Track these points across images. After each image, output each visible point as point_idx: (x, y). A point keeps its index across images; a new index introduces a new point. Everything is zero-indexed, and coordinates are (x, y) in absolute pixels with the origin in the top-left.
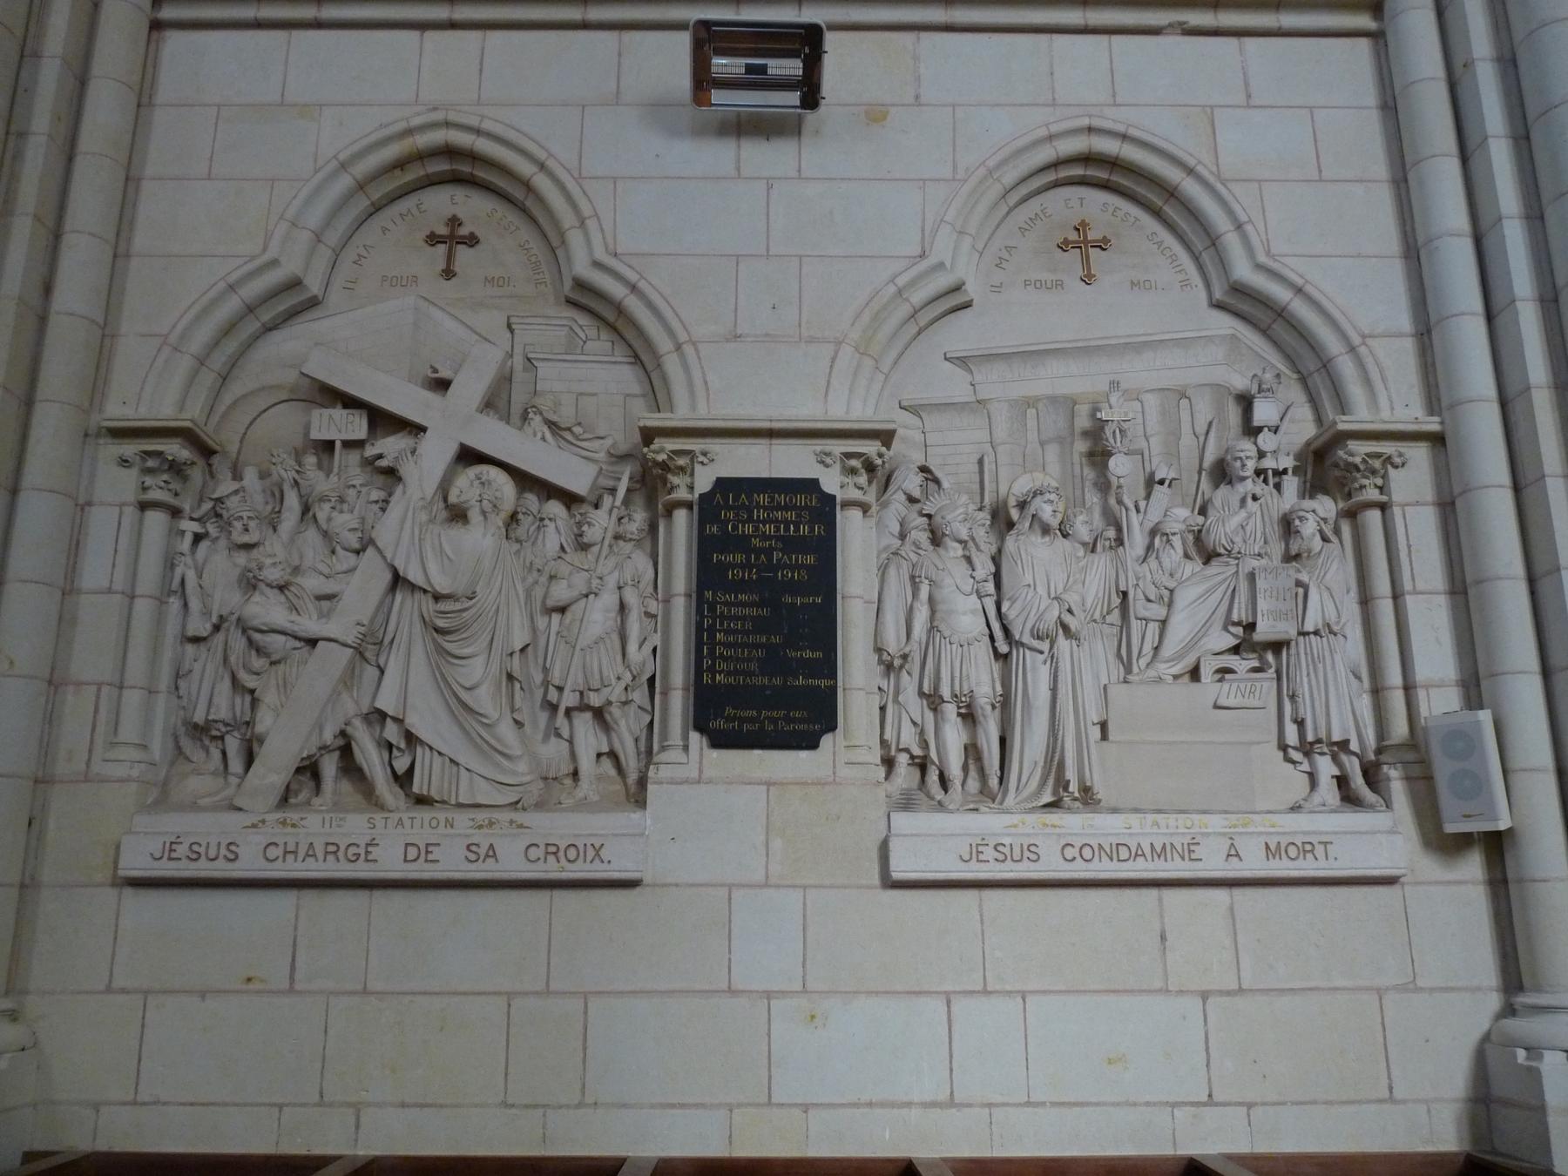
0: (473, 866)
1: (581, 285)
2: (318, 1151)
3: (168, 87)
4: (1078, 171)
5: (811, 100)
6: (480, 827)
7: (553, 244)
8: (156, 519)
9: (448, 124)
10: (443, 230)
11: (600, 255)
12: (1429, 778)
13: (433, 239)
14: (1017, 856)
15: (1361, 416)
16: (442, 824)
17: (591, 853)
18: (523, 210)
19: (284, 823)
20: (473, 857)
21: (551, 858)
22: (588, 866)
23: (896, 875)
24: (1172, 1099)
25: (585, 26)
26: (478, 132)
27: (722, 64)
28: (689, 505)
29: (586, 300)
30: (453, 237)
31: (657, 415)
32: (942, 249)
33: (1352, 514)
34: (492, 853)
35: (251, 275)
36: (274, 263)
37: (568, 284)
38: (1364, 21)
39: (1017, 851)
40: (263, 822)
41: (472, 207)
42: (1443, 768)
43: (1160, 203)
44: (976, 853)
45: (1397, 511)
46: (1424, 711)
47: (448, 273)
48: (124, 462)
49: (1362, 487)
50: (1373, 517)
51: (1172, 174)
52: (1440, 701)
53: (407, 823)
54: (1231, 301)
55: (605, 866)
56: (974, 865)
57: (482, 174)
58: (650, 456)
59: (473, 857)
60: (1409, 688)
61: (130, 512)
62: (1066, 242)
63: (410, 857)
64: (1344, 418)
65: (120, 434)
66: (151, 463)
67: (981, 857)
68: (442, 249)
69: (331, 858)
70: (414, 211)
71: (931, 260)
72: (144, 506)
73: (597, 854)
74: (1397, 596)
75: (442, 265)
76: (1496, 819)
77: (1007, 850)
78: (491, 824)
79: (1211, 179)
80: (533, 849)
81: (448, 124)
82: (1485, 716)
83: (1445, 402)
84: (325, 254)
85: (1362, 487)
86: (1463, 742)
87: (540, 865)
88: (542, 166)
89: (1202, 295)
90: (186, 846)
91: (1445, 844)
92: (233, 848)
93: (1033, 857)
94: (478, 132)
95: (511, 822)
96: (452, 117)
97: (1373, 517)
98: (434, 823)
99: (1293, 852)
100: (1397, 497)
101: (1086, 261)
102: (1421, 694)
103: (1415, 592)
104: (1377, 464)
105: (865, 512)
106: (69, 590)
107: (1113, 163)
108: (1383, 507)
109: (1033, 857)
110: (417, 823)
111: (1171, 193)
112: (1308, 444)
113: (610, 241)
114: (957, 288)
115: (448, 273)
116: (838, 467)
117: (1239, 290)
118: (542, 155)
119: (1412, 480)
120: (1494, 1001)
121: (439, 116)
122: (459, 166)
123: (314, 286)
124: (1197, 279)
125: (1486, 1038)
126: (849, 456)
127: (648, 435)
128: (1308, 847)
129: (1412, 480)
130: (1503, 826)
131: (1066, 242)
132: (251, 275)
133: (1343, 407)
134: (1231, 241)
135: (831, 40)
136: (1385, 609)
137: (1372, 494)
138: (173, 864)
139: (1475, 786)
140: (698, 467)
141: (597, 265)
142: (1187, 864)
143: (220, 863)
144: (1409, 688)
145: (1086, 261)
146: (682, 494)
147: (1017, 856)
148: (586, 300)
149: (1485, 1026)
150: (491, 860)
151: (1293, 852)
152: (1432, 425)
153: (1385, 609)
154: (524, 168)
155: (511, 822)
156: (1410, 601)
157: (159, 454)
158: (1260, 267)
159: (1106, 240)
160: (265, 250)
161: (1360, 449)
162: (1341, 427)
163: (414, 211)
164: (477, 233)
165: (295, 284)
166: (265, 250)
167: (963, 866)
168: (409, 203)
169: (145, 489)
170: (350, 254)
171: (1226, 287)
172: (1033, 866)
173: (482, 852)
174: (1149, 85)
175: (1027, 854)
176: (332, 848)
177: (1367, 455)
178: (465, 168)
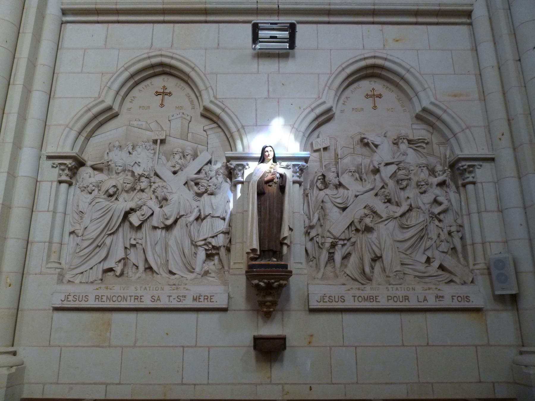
0: (319, 304)
1: (206, 109)
2: (81, 398)
3: (66, 43)
4: (370, 71)
5: (292, 46)
6: (426, 290)
7: (198, 96)
8: (64, 186)
13: (158, 94)
14: (337, 300)
16: (160, 289)
18: (187, 83)
19: (107, 288)
20: (153, 300)
21: (206, 300)
23: (311, 307)
24: (194, 383)
25: (206, 22)
26: (172, 58)
28: (242, 183)
29: (208, 115)
30: (164, 93)
34: (425, 299)
35: (97, 105)
36: (103, 101)
37: (202, 108)
40: (100, 288)
41: (170, 83)
44: (67, 297)
51: (403, 72)
55: (378, 304)
56: (322, 303)
58: (229, 165)
59: (153, 300)
61: (55, 184)
62: (367, 95)
65: (50, 158)
66: (62, 167)
68: (160, 97)
69: (407, 301)
70: (150, 85)
71: (100, 99)
72: (60, 182)
77: (77, 298)
79: (417, 75)
81: (161, 55)
84: (119, 98)
88: (193, 69)
90: (72, 296)
94: (386, 59)
96: (163, 53)
100: (479, 179)
103: (486, 211)
105: (300, 185)
106: (501, 210)
109: (343, 301)
110: (151, 288)
113: (215, 93)
114: (329, 110)
115: (162, 105)
118: (193, 66)
121: (159, 53)
122: (163, 69)
123: (116, 108)
126: (61, 164)
127: (229, 159)
131: (367, 95)
132: (97, 105)
135: (299, 27)
137: (471, 179)
138: (69, 303)
140: (477, 170)
141: (211, 102)
142: (210, 303)
143: (83, 302)
146: (240, 179)
148: (208, 115)
155: (184, 288)
157: (65, 164)
158: (211, 102)
159: (170, 93)
160: (99, 97)
162: (460, 156)
163: (150, 85)
165: (110, 108)
170: (128, 99)
173: (156, 299)
175: (340, 299)
176: (407, 298)
178: (167, 70)
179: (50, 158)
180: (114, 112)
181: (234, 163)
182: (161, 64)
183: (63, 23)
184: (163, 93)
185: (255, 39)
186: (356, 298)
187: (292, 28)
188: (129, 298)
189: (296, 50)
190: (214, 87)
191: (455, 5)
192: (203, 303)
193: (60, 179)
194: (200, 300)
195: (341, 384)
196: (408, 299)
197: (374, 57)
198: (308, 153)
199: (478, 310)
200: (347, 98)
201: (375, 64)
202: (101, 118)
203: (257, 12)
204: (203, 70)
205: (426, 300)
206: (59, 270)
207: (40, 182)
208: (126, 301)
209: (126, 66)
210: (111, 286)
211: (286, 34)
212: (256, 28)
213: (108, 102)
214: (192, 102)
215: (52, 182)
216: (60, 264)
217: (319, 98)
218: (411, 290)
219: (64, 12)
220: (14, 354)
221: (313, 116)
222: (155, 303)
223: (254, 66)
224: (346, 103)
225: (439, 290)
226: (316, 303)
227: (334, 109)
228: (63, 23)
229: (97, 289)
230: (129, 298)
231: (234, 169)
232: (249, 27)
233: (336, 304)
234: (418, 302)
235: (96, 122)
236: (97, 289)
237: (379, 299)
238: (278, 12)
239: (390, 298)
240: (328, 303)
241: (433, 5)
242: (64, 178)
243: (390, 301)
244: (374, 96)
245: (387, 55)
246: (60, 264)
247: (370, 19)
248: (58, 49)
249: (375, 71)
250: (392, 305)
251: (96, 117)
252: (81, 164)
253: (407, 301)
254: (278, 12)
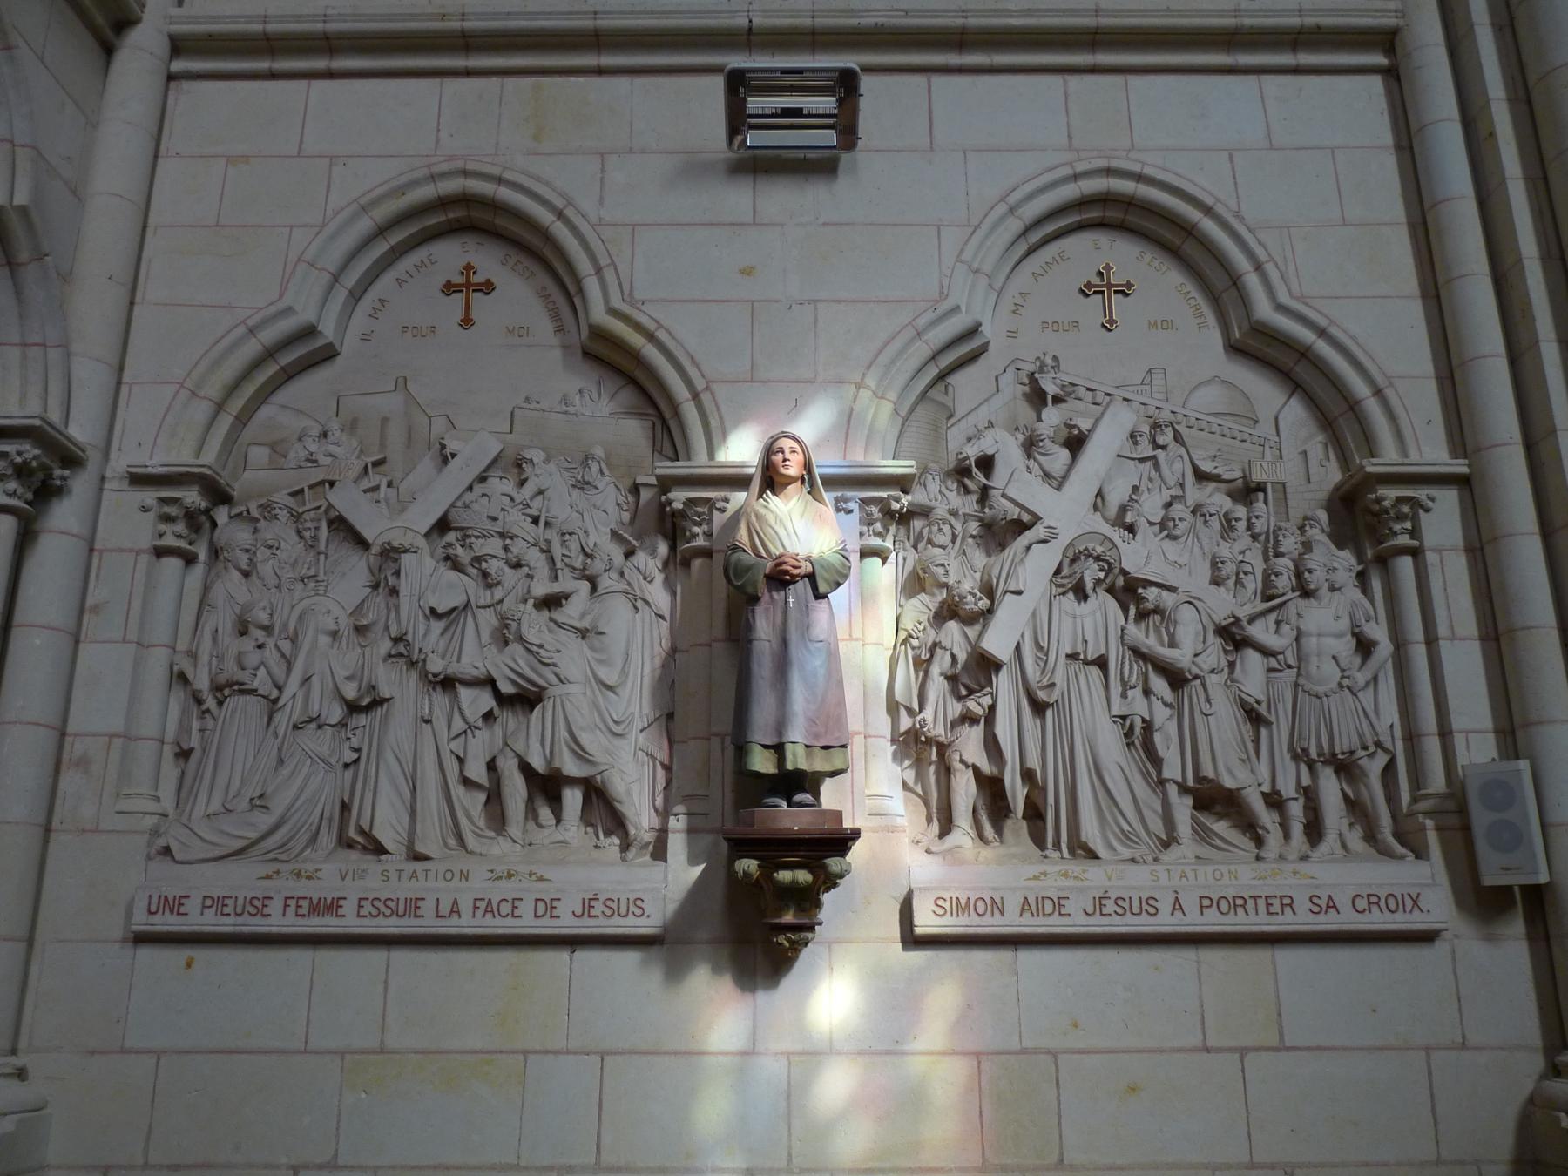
0: (1091, 920)
8: (174, 563)
9: (465, 173)
10: (459, 280)
11: (616, 303)
12: (1467, 828)
13: (449, 288)
14: (623, 911)
15: (1388, 458)
16: (457, 875)
17: (1409, 903)
19: (1066, 875)
21: (1375, 908)
22: (1407, 917)
23: (918, 931)
26: (500, 180)
27: (755, 104)
30: (468, 286)
31: (896, 462)
32: (958, 296)
33: (1383, 561)
36: (289, 311)
37: (585, 333)
38: (1380, 59)
39: (1136, 904)
40: (278, 872)
41: (487, 260)
42: (1481, 818)
43: (1178, 242)
45: (1431, 557)
46: (1462, 759)
47: (467, 322)
48: (145, 509)
49: (694, 536)
50: (1405, 564)
51: (1193, 214)
52: (1478, 749)
53: (421, 875)
54: (1253, 344)
56: (1097, 919)
57: (501, 222)
59: (1316, 909)
60: (1445, 734)
62: (1089, 285)
63: (540, 912)
64: (1374, 461)
65: (139, 480)
67: (593, 912)
71: (281, 305)
72: (160, 552)
73: (1415, 902)
74: (1431, 641)
75: (460, 315)
76: (1536, 872)
78: (510, 876)
80: (1358, 900)
81: (465, 173)
82: (1524, 764)
83: (1469, 448)
85: (694, 536)
86: (1501, 793)
87: (1366, 917)
89: (1216, 337)
91: (1486, 903)
92: (639, 903)
93: (1152, 911)
94: (500, 180)
95: (531, 874)
97: (1405, 564)
98: (1218, 875)
99: (1224, 906)
101: (1107, 308)
102: (69, 739)
104: (1406, 509)
107: (1129, 203)
108: (1416, 553)
109: (1152, 911)
110: (432, 875)
111: (1188, 230)
112: (1337, 488)
114: (973, 331)
115: (467, 322)
116: (856, 515)
117: (1264, 332)
119: (1442, 522)
120: (1538, 1062)
121: (459, 164)
123: (328, 330)
124: (1211, 319)
125: (1531, 1100)
127: (666, 484)
128: (1373, 899)
129: (1442, 522)
130: (1543, 878)
131: (1089, 285)
133: (1371, 449)
134: (1252, 281)
135: (867, 83)
136: (1419, 653)
137: (1404, 540)
139: (1510, 838)
144: (1445, 734)
145: (1107, 308)
147: (623, 911)
149: (1528, 1086)
150: (455, 916)
151: (1224, 906)
152: (1460, 467)
153: (1419, 653)
154: (544, 216)
156: (1445, 647)
157: (174, 501)
160: (281, 296)
161: (1390, 494)
162: (1370, 469)
164: (494, 280)
165: (310, 332)
166: (281, 296)
167: (577, 922)
168: (421, 254)
169: (161, 536)
171: (1246, 326)
172: (1151, 920)
174: (1174, 130)
175: (632, 908)
177: (1400, 500)
179: (139, 480)
180: (320, 342)
181: (679, 497)
182: (464, 200)
183: (171, 77)
184: (468, 284)
185: (737, 121)
186: (1261, 903)
187: (846, 84)
188: (1251, 903)
189: (861, 155)
190: (623, 269)
191: (1168, 12)
192: (1280, 919)
193: (158, 543)
194: (1272, 910)
195: (161, 1167)
196: (1290, 905)
197: (1109, 172)
198: (912, 463)
199: (1426, 937)
200: (382, 302)
201: (1083, 197)
202: (286, 359)
203: (749, 38)
204: (1233, 205)
205: (458, 912)
206: (155, 819)
207: (101, 552)
208: (1002, 914)
209: (363, 201)
210: (310, 867)
211: (827, 103)
212: (737, 83)
213: (306, 315)
214: (555, 316)
215: (138, 552)
216: (158, 799)
217: (943, 296)
218: (1226, 877)
219: (179, 46)
220: (21, 1074)
221: (922, 350)
222: (1322, 918)
223: (738, 197)
224: (1021, 310)
225: (541, 879)
226: (1083, 919)
227: (986, 329)
228: (171, 77)
229: (268, 877)
230: (1251, 903)
231: (681, 514)
232: (718, 83)
233: (622, 921)
234: (536, 916)
235: (270, 370)
236: (268, 877)
237: (1069, 907)
238: (815, 39)
239: (1206, 902)
240: (602, 921)
241: (1221, 13)
242: (170, 541)
243: (206, 911)
244: (468, 286)
245: (1144, 164)
246: (158, 799)
247: (320, 64)
248: (156, 156)
249: (1108, 214)
250: (1098, 926)
251: (270, 354)
252: (219, 495)
253: (1288, 909)
254: (815, 39)
